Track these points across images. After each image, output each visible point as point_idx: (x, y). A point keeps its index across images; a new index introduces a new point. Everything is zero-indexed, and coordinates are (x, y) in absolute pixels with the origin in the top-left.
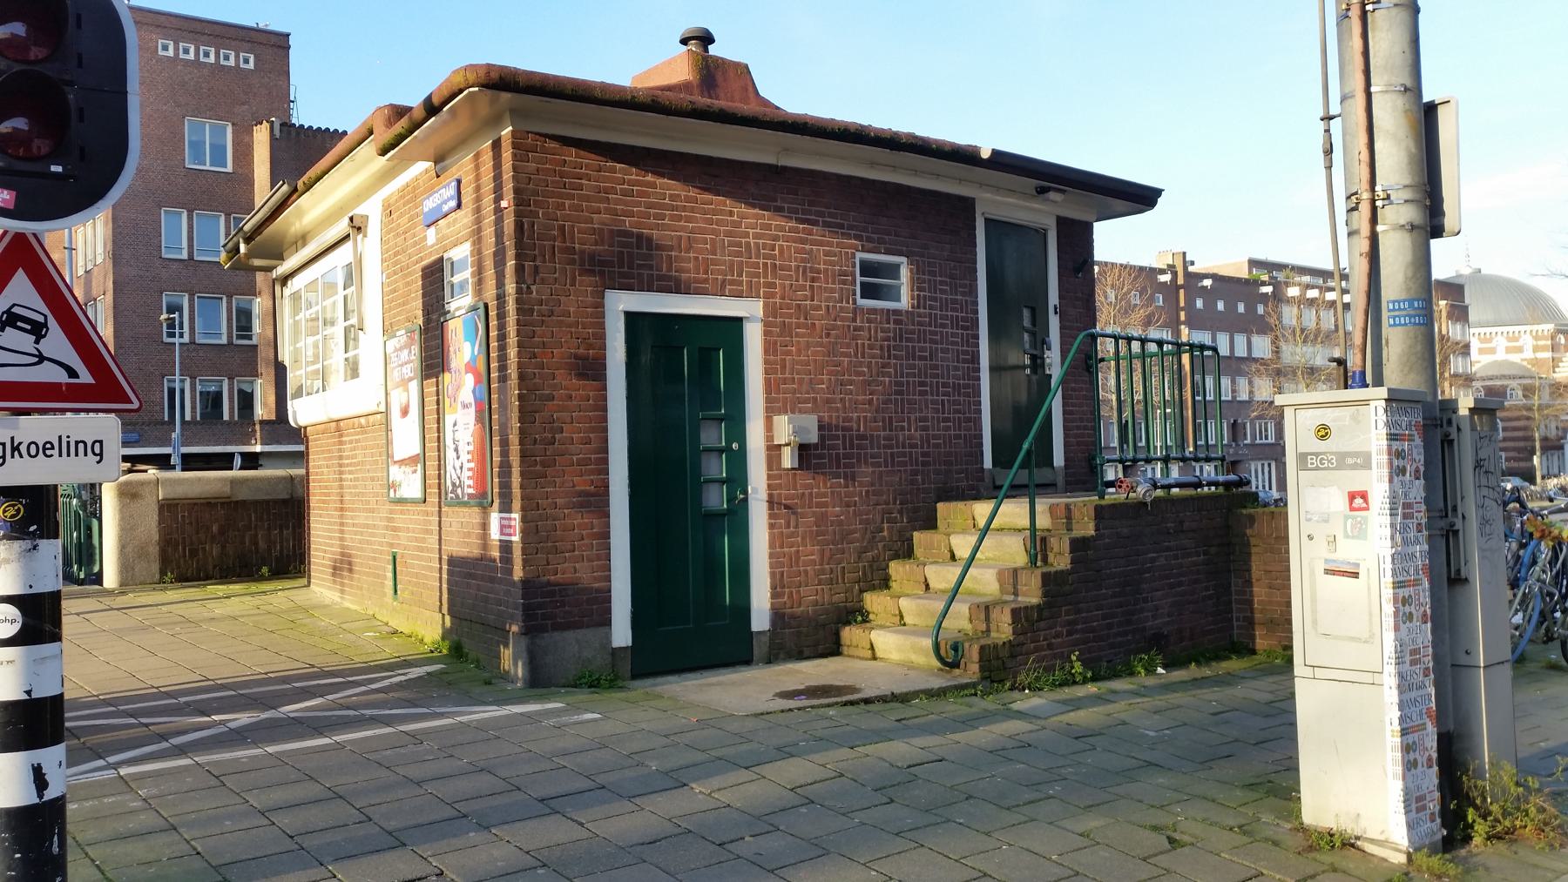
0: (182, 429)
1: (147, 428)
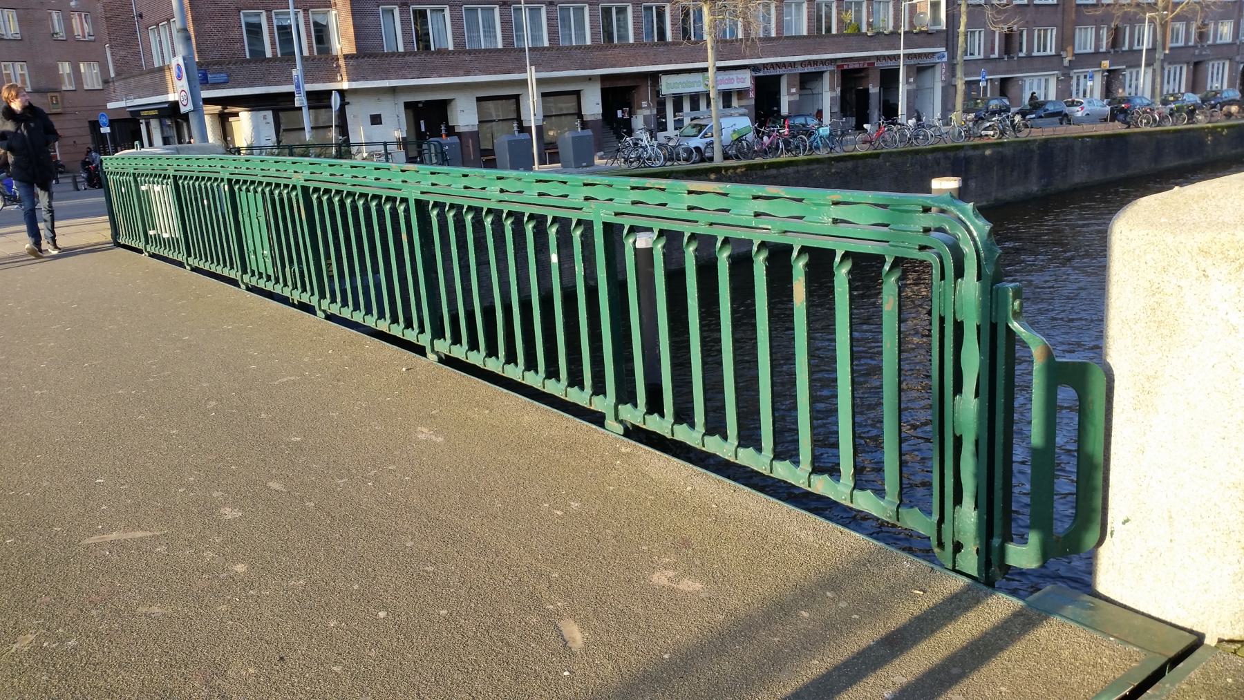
0: (304, 67)
1: (234, 67)
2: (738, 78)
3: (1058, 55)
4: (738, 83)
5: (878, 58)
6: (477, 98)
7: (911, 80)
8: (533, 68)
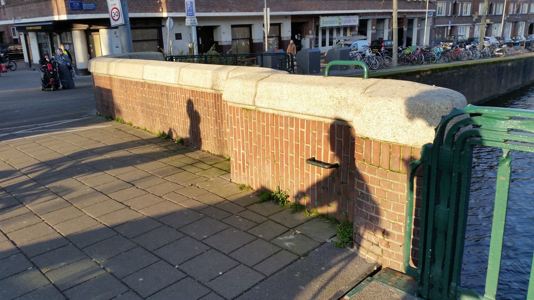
2: (353, 20)
3: (471, 16)
4: (353, 22)
5: (407, 13)
6: (231, 25)
7: (374, 27)
8: (268, 9)
